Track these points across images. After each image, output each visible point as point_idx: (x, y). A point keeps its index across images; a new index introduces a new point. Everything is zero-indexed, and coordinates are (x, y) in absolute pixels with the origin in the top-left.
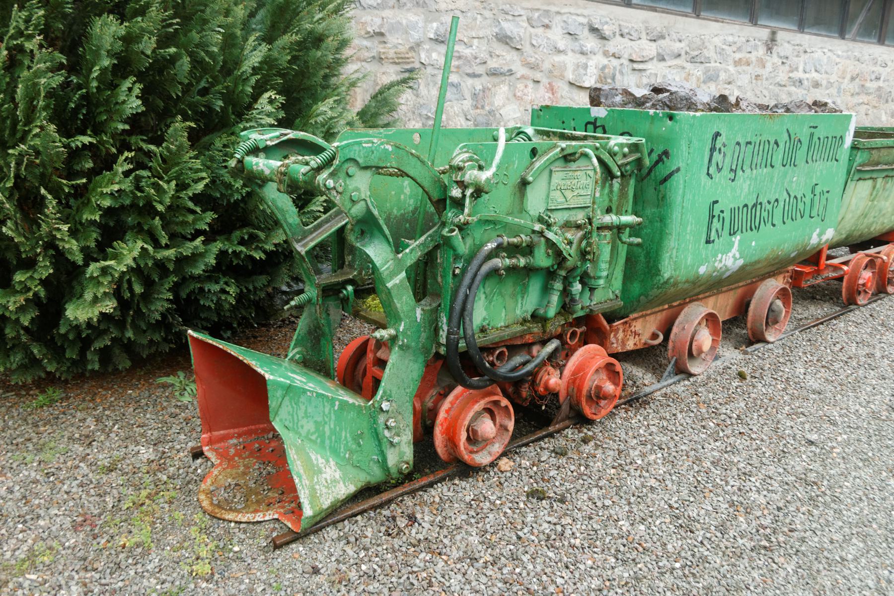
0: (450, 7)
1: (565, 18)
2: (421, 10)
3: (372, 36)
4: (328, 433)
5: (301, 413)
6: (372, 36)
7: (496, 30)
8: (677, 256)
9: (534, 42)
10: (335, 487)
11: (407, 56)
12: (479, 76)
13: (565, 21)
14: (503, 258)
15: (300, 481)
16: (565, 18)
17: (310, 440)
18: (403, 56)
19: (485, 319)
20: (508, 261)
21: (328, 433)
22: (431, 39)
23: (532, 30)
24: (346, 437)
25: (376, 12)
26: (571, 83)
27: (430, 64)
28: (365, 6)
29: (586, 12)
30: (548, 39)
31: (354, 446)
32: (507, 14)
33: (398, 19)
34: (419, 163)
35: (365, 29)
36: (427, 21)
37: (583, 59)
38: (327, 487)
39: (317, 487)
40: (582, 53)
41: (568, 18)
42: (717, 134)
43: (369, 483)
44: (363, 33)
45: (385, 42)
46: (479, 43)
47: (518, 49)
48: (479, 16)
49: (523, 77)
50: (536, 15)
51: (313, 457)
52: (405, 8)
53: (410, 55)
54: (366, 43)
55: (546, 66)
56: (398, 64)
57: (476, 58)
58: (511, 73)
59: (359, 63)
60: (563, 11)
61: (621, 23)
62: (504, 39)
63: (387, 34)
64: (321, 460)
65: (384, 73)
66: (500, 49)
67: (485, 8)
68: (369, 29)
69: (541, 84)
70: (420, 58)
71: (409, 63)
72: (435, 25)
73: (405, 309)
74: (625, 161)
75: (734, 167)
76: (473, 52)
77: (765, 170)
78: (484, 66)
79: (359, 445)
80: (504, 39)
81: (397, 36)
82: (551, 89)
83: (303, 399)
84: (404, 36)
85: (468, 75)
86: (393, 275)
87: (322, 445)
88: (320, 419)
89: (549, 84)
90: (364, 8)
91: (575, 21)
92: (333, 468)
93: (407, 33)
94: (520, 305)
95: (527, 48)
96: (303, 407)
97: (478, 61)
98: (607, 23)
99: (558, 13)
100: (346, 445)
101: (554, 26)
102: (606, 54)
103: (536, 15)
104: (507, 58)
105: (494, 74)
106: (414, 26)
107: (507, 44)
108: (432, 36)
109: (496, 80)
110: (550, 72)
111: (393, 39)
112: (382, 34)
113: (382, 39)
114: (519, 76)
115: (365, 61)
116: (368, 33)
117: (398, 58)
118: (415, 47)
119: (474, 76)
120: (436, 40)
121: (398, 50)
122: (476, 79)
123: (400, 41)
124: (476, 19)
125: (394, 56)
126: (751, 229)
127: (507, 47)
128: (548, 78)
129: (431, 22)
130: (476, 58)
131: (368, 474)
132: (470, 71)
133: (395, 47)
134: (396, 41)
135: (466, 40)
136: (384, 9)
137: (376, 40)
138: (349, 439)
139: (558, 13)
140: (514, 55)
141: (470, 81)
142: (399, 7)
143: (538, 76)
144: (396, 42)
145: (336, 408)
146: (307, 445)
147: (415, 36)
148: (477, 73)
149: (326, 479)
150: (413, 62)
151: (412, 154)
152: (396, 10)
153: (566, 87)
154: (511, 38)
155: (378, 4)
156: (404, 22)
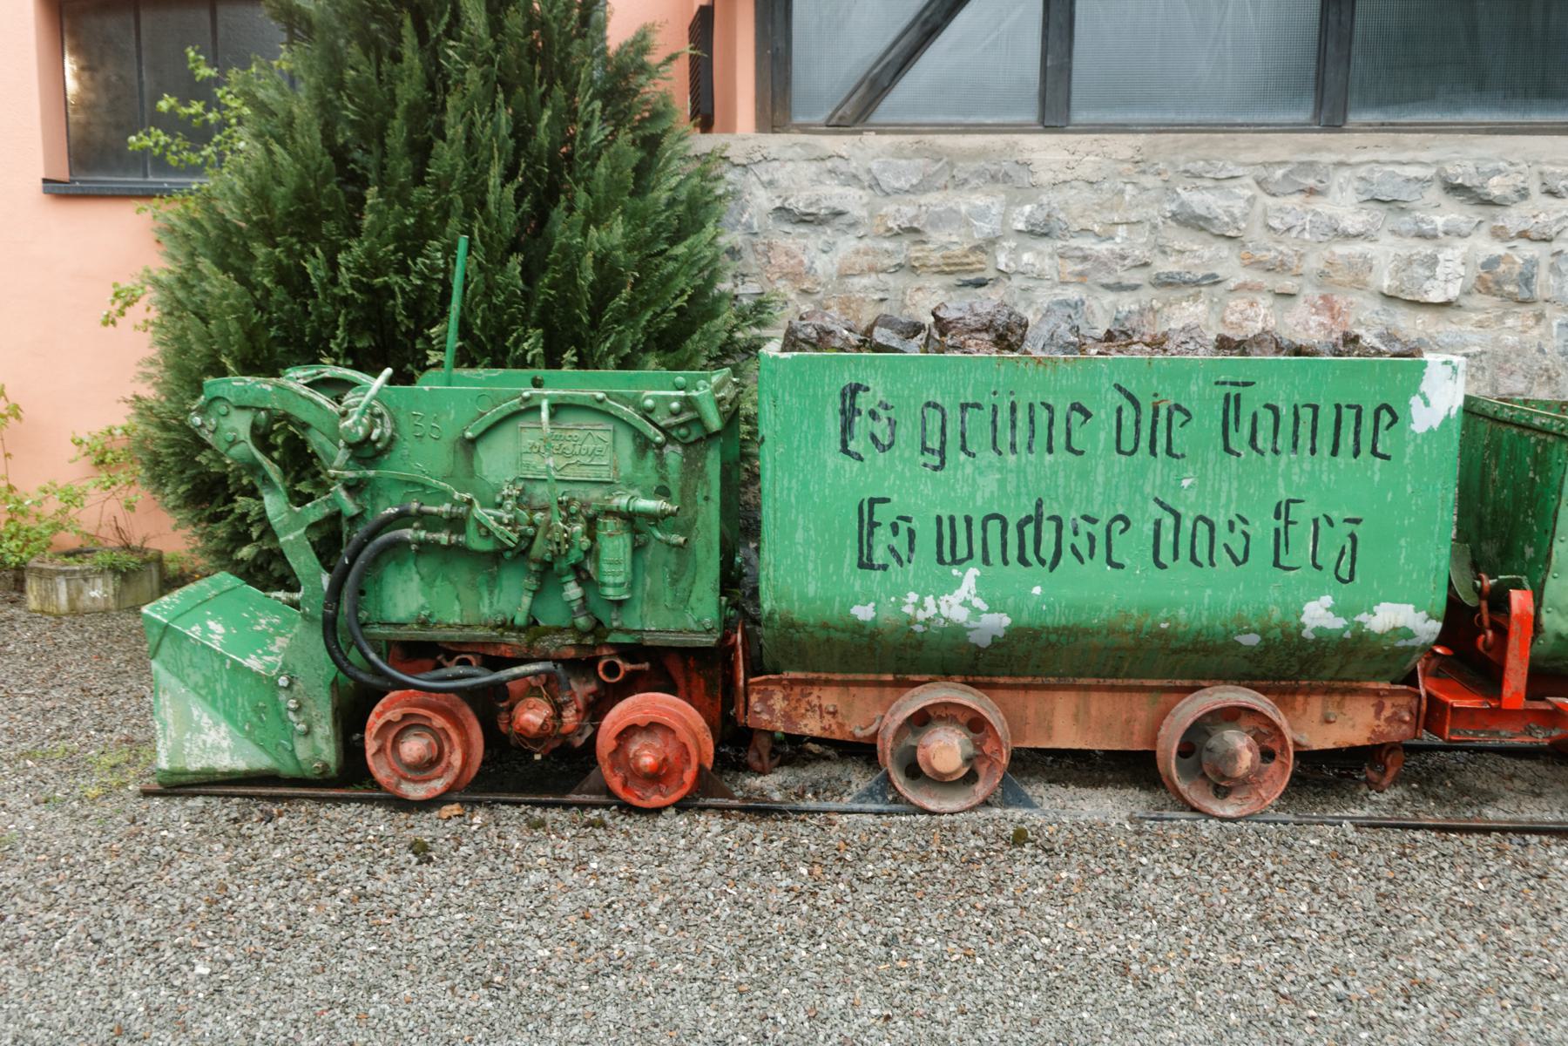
0: (1061, 177)
1: (1362, 172)
2: (1000, 186)
3: (898, 234)
4: (220, 693)
5: (186, 661)
6: (898, 234)
7: (1171, 207)
8: (775, 578)
9: (1275, 223)
10: (215, 754)
11: (966, 260)
12: (1135, 288)
13: (1362, 179)
14: (416, 529)
15: (164, 729)
16: (1362, 172)
17: (199, 694)
18: (957, 261)
19: (423, 608)
20: (422, 534)
21: (220, 693)
22: (1020, 231)
23: (1270, 201)
24: (243, 705)
25: (912, 197)
26: (1390, 298)
27: (1017, 272)
28: (889, 191)
29: (1425, 156)
30: (1316, 214)
31: (255, 720)
32: (1200, 177)
33: (951, 204)
34: (313, 406)
35: (885, 224)
36: (1011, 203)
37: (1426, 248)
38: (204, 751)
39: (188, 745)
40: (1422, 235)
41: (1372, 171)
42: (855, 389)
43: (278, 771)
44: (882, 230)
45: (924, 242)
46: (1130, 232)
47: (1230, 238)
48: (1129, 187)
49: (1243, 287)
50: (1279, 173)
51: (196, 713)
52: (967, 187)
53: (972, 258)
54: (888, 245)
55: (1313, 263)
56: (951, 273)
57: (1123, 258)
58: (1214, 280)
59: (873, 276)
60: (1353, 160)
61: (1548, 169)
62: (1195, 222)
63: (928, 229)
64: (205, 719)
65: (919, 289)
66: (1180, 239)
67: (1144, 172)
68: (891, 224)
69: (1300, 301)
70: (997, 263)
71: (972, 272)
72: (1027, 209)
73: (304, 571)
74: (673, 421)
75: (934, 443)
76: (1117, 249)
77: (1048, 458)
78: (1146, 270)
79: (261, 718)
80: (1195, 222)
81: (948, 230)
82: (1328, 305)
83: (185, 644)
84: (963, 231)
85: (1107, 287)
86: (288, 529)
87: (213, 704)
88: (209, 674)
89: (1323, 297)
90: (888, 194)
91: (1393, 175)
92: (223, 734)
93: (968, 224)
94: (486, 601)
95: (1257, 234)
96: (187, 654)
97: (1128, 262)
98: (1499, 172)
99: (1341, 164)
100: (245, 713)
101: (1334, 188)
102: (1498, 234)
103: (1279, 173)
104: (1201, 254)
105: (1171, 284)
106: (983, 214)
107: (1202, 229)
108: (1021, 226)
109: (1173, 294)
110: (1322, 274)
111: (938, 237)
112: (916, 231)
113: (918, 237)
114: (1232, 286)
115: (884, 271)
116: (890, 229)
117: (948, 265)
118: (991, 243)
119: (1119, 287)
120: (1031, 232)
121: (948, 253)
122: (1125, 294)
123: (954, 238)
124: (1121, 192)
125: (941, 261)
126: (1023, 560)
127: (1203, 235)
128: (1319, 287)
129: (1021, 203)
130: (1123, 258)
131: (277, 760)
132: (1111, 280)
133: (944, 247)
134: (945, 239)
135: (1097, 228)
136: (926, 191)
137: (906, 241)
138: (248, 709)
139: (1341, 164)
140: (1224, 249)
141: (1109, 298)
142: (956, 186)
143: (1288, 284)
144: (947, 240)
145: (228, 667)
146: (193, 697)
147: (985, 228)
148: (1125, 282)
149: (204, 743)
150: (982, 270)
151: (301, 396)
152: (950, 192)
153: (1376, 305)
154: (1206, 219)
155: (912, 186)
156: (963, 208)
